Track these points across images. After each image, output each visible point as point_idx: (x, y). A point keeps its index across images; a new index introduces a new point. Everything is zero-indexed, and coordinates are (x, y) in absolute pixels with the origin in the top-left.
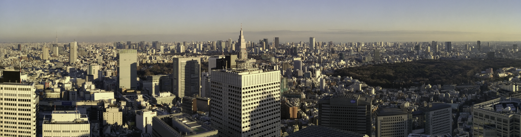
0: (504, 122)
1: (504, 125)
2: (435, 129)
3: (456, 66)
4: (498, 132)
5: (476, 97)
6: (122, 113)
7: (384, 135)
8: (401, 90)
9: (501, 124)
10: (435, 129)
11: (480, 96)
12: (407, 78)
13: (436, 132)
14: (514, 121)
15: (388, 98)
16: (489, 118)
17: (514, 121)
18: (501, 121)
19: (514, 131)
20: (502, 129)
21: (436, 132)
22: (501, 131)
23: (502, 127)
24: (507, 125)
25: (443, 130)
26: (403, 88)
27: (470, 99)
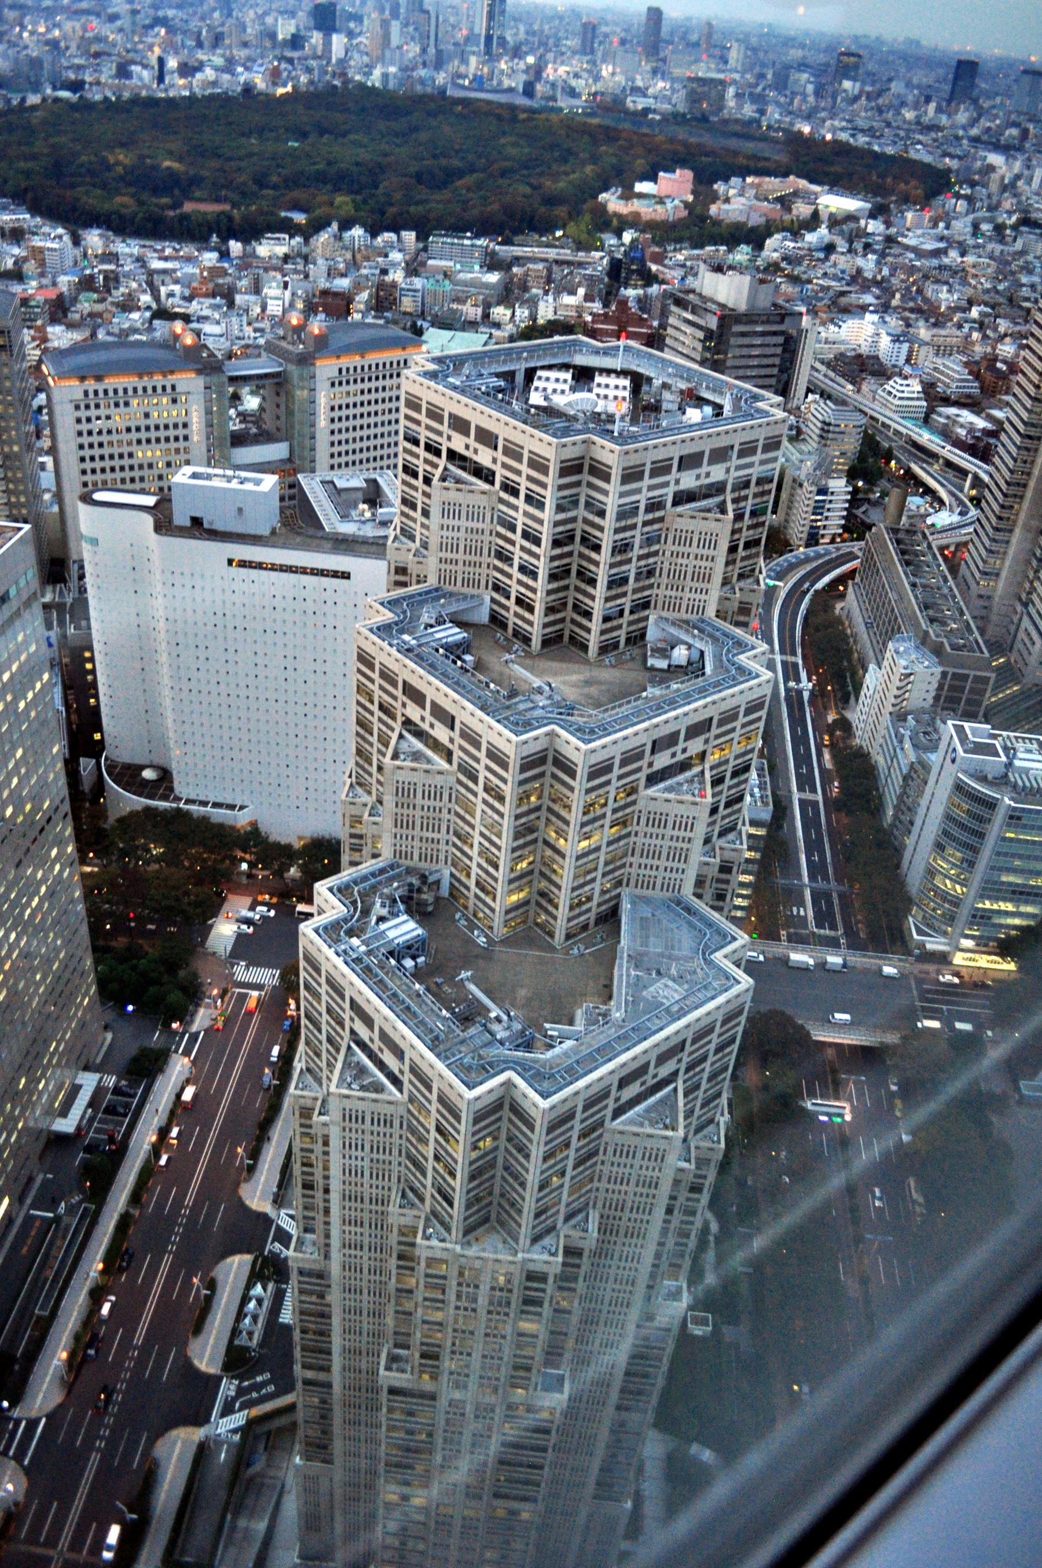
0: (533, 464)
1: (530, 478)
2: (343, 448)
3: (792, 52)
4: (504, 509)
5: (579, 309)
6: (661, 174)
7: (148, 441)
8: (212, 250)
9: (518, 473)
10: (343, 448)
11: (597, 307)
12: (255, 188)
13: (343, 459)
14: (586, 468)
15: (144, 291)
16: (468, 435)
17: (586, 468)
18: (518, 458)
19: (580, 520)
20: (522, 496)
21: (343, 459)
22: (515, 508)
23: (524, 485)
24: (544, 486)
25: (379, 453)
26: (225, 240)
27: (551, 316)
